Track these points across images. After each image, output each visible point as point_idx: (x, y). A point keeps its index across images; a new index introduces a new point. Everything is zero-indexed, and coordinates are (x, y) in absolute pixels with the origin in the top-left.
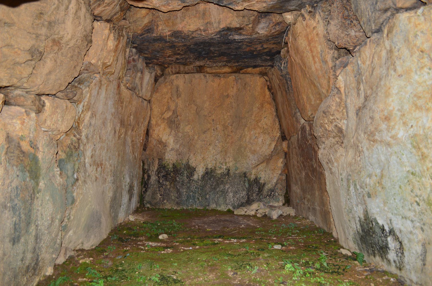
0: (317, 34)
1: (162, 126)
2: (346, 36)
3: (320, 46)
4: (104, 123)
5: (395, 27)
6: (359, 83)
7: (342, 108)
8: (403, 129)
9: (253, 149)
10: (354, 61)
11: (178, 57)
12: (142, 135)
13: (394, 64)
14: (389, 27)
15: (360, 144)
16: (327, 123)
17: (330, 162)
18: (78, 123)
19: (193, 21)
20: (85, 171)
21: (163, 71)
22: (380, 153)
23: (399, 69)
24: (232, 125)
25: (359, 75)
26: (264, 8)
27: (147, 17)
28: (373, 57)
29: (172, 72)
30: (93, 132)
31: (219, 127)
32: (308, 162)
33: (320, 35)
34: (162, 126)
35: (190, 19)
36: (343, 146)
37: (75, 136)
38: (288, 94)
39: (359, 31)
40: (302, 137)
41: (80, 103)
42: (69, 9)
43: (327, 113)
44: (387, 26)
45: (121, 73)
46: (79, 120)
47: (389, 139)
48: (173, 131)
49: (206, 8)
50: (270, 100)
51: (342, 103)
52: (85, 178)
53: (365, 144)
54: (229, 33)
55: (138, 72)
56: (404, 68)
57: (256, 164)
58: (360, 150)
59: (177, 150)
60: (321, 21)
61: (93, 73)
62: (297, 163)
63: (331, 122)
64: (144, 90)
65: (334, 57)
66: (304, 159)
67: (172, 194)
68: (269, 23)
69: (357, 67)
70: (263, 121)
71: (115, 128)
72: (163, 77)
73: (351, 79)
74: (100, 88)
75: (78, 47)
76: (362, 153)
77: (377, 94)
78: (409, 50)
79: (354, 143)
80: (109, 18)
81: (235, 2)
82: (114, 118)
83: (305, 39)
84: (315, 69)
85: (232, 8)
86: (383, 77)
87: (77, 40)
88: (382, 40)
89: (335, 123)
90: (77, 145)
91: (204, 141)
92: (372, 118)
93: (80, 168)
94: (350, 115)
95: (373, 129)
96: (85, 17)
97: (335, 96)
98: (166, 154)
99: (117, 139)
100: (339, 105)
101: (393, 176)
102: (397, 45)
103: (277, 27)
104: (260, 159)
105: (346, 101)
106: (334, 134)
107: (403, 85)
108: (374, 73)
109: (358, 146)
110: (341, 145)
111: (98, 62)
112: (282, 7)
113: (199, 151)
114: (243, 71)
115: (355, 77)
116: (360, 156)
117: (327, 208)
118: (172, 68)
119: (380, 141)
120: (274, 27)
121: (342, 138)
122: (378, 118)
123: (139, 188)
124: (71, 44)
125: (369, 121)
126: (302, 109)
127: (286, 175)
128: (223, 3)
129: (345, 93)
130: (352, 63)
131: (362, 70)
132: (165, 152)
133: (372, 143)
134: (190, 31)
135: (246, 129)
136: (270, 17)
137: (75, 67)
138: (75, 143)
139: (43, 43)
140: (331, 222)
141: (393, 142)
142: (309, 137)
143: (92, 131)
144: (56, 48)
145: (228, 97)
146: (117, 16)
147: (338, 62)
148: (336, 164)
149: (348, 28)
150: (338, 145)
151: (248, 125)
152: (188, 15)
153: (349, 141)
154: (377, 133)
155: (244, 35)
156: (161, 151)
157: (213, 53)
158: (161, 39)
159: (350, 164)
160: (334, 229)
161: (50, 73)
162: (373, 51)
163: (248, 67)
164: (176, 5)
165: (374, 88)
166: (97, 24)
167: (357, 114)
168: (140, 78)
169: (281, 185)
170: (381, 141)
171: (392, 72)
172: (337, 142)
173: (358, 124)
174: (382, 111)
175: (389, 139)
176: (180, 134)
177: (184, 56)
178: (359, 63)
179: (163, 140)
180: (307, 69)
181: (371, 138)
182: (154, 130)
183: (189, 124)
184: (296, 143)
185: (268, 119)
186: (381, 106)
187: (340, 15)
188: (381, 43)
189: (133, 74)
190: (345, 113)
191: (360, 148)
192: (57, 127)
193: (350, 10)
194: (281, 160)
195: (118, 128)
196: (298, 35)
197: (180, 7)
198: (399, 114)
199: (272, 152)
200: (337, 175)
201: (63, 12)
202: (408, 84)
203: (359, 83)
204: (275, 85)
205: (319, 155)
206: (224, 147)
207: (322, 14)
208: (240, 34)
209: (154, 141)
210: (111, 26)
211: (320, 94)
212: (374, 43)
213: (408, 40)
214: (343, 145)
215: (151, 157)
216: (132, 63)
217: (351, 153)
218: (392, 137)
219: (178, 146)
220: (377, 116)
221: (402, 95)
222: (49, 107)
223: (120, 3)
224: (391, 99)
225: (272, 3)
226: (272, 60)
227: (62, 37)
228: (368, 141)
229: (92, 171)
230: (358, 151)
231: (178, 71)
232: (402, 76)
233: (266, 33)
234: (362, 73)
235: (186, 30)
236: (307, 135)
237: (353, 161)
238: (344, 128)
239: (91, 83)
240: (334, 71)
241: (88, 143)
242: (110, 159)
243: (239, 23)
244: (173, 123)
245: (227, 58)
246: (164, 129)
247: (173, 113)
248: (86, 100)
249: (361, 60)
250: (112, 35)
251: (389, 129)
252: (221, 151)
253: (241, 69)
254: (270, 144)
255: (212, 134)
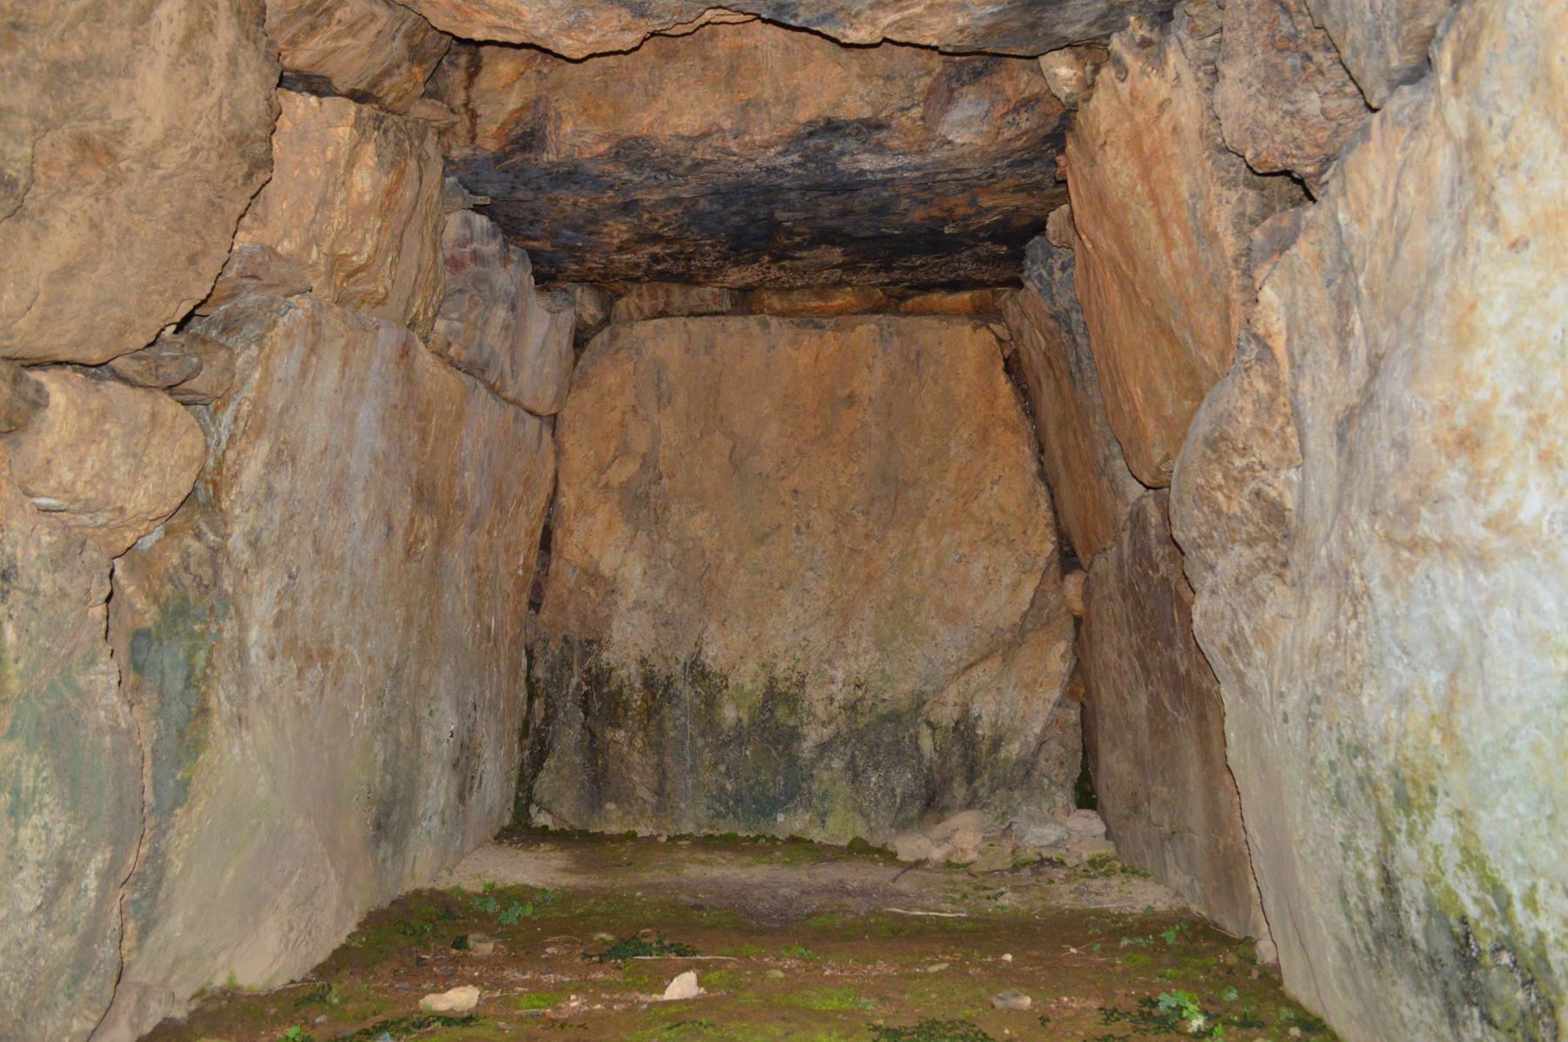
0: (1174, 129)
1: (602, 515)
2: (1288, 120)
3: (1188, 174)
4: (338, 494)
5: (1486, 32)
6: (1343, 307)
7: (1280, 420)
8: (1539, 486)
9: (949, 602)
10: (1321, 218)
11: (657, 249)
12: (522, 548)
13: (1486, 195)
14: (1459, 38)
15: (1354, 566)
16: (1220, 487)
17: (1237, 645)
18: (215, 484)
19: (692, 97)
20: (243, 681)
21: (607, 304)
22: (1447, 596)
23: (1511, 214)
24: (866, 513)
25: (1345, 273)
26: (961, 31)
27: (517, 86)
28: (1398, 185)
29: (640, 310)
30: (282, 524)
31: (822, 521)
32: (1159, 653)
33: (1186, 132)
34: (602, 515)
35: (679, 90)
36: (1288, 580)
37: (198, 536)
38: (1079, 387)
39: (1339, 91)
40: (1134, 554)
41: (225, 405)
42: (154, 22)
43: (1222, 446)
44: (1453, 34)
45: (418, 302)
46: (220, 473)
47: (1481, 533)
48: (642, 535)
49: (740, 48)
50: (1014, 414)
51: (1281, 400)
52: (245, 705)
53: (1375, 564)
54: (837, 148)
55: (495, 301)
56: (1536, 209)
57: (964, 664)
58: (1358, 589)
59: (658, 609)
60: (1187, 76)
61: (282, 291)
62: (1120, 656)
63: (1236, 480)
64: (525, 376)
65: (1243, 214)
66: (1143, 639)
67: (636, 778)
68: (992, 104)
69: (1334, 241)
70: (986, 495)
71: (388, 516)
72: (606, 332)
73: (1315, 293)
74: (313, 350)
75: (208, 181)
76: (1366, 601)
77: (1419, 337)
78: (1554, 122)
79: (1331, 563)
80: (361, 86)
81: (842, 9)
82: (386, 473)
83: (1127, 154)
84: (1170, 273)
85: (832, 34)
86: (1442, 261)
87: (196, 151)
88: (1433, 104)
89: (1253, 485)
90: (206, 573)
91: (761, 572)
92: (1400, 446)
93: (219, 664)
94: (1312, 445)
95: (1406, 495)
96: (232, 60)
97: (1252, 373)
98: (615, 624)
99: (399, 554)
100: (1267, 407)
101: (1503, 700)
102: (1499, 110)
103: (1024, 116)
104: (977, 645)
105: (1294, 391)
106: (1251, 528)
107: (1533, 285)
108: (1405, 252)
109: (1347, 574)
110: (1279, 575)
111: (306, 247)
112: (1033, 26)
113: (740, 612)
114: (910, 302)
115: (1329, 283)
116: (1355, 615)
117: (1235, 838)
118: (640, 296)
119: (1440, 546)
120: (1010, 118)
121: (1283, 547)
122: (1428, 440)
123: (509, 754)
124: (171, 160)
125: (1390, 460)
126: (1130, 441)
127: (1082, 705)
128: (795, 16)
129: (1291, 356)
130: (1313, 225)
131: (1354, 249)
132: (609, 616)
133: (1405, 554)
134: (682, 138)
135: (922, 527)
136: (995, 80)
137: (192, 260)
138: (200, 564)
139: (21, 144)
140: (1250, 896)
141: (1495, 542)
142: (1159, 552)
143: (277, 518)
144: (95, 175)
145: (852, 404)
146: (396, 79)
147: (1258, 235)
148: (1259, 654)
149: (1295, 86)
150: (1268, 576)
151: (929, 513)
152: (674, 76)
153: (1310, 556)
154: (1424, 512)
155: (895, 153)
156: (594, 612)
157: (790, 233)
158: (570, 175)
159: (1317, 653)
160: (1265, 928)
161: (67, 272)
162: (1398, 157)
163: (927, 288)
164: (613, 29)
165: (1407, 315)
166: (300, 105)
167: (1341, 439)
168: (506, 328)
169: (1062, 744)
170: (1445, 546)
171: (1483, 235)
172: (1265, 561)
173: (1345, 480)
174: (1446, 409)
175: (1481, 533)
176: (668, 545)
177: (676, 247)
178: (1342, 223)
179: (605, 570)
180: (1140, 272)
181: (1401, 535)
182: (571, 532)
183: (703, 508)
184: (1111, 579)
185: (1009, 485)
186: (1438, 386)
187: (1262, 35)
188: (1430, 117)
189: (471, 310)
190: (1295, 441)
191: (1357, 581)
192: (108, 497)
193: (1300, 12)
194: (1062, 647)
195: (401, 517)
196: (1100, 142)
197: (630, 39)
198: (1520, 416)
199: (1025, 615)
200: (1266, 700)
201: (126, 33)
202: (1555, 277)
203: (1343, 307)
204: (1033, 352)
205: (1196, 617)
206: (836, 598)
207: (1190, 44)
208: (880, 148)
209: (570, 571)
210: (365, 114)
211: (1193, 373)
212: (1399, 124)
213: (1548, 79)
214: (1290, 575)
215: (560, 636)
216: (472, 268)
217: (1320, 604)
218: (1492, 523)
219: (661, 591)
220: (1423, 434)
221: (1529, 329)
222: (61, 409)
223: (404, 28)
224: (1480, 355)
225: (990, 9)
226: (1017, 258)
227: (122, 133)
228: (1388, 549)
229: (280, 680)
230: (1352, 598)
231: (661, 307)
232: (1527, 244)
233: (979, 141)
234: (1356, 262)
235: (664, 133)
236: (1154, 542)
237: (1331, 637)
238: (1290, 502)
239: (271, 327)
240: (1248, 273)
241: (260, 564)
242: (366, 633)
243: (871, 104)
244: (641, 505)
245: (844, 254)
246: (610, 527)
247: (644, 467)
248: (249, 392)
249: (1348, 206)
250: (370, 149)
251: (1474, 492)
252: (828, 614)
253: (902, 298)
254: (1016, 586)
255: (792, 547)
